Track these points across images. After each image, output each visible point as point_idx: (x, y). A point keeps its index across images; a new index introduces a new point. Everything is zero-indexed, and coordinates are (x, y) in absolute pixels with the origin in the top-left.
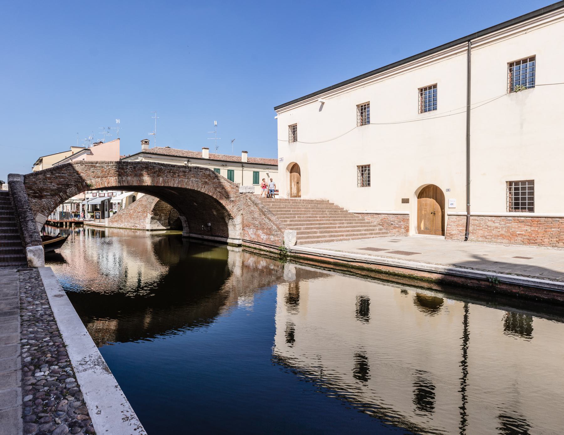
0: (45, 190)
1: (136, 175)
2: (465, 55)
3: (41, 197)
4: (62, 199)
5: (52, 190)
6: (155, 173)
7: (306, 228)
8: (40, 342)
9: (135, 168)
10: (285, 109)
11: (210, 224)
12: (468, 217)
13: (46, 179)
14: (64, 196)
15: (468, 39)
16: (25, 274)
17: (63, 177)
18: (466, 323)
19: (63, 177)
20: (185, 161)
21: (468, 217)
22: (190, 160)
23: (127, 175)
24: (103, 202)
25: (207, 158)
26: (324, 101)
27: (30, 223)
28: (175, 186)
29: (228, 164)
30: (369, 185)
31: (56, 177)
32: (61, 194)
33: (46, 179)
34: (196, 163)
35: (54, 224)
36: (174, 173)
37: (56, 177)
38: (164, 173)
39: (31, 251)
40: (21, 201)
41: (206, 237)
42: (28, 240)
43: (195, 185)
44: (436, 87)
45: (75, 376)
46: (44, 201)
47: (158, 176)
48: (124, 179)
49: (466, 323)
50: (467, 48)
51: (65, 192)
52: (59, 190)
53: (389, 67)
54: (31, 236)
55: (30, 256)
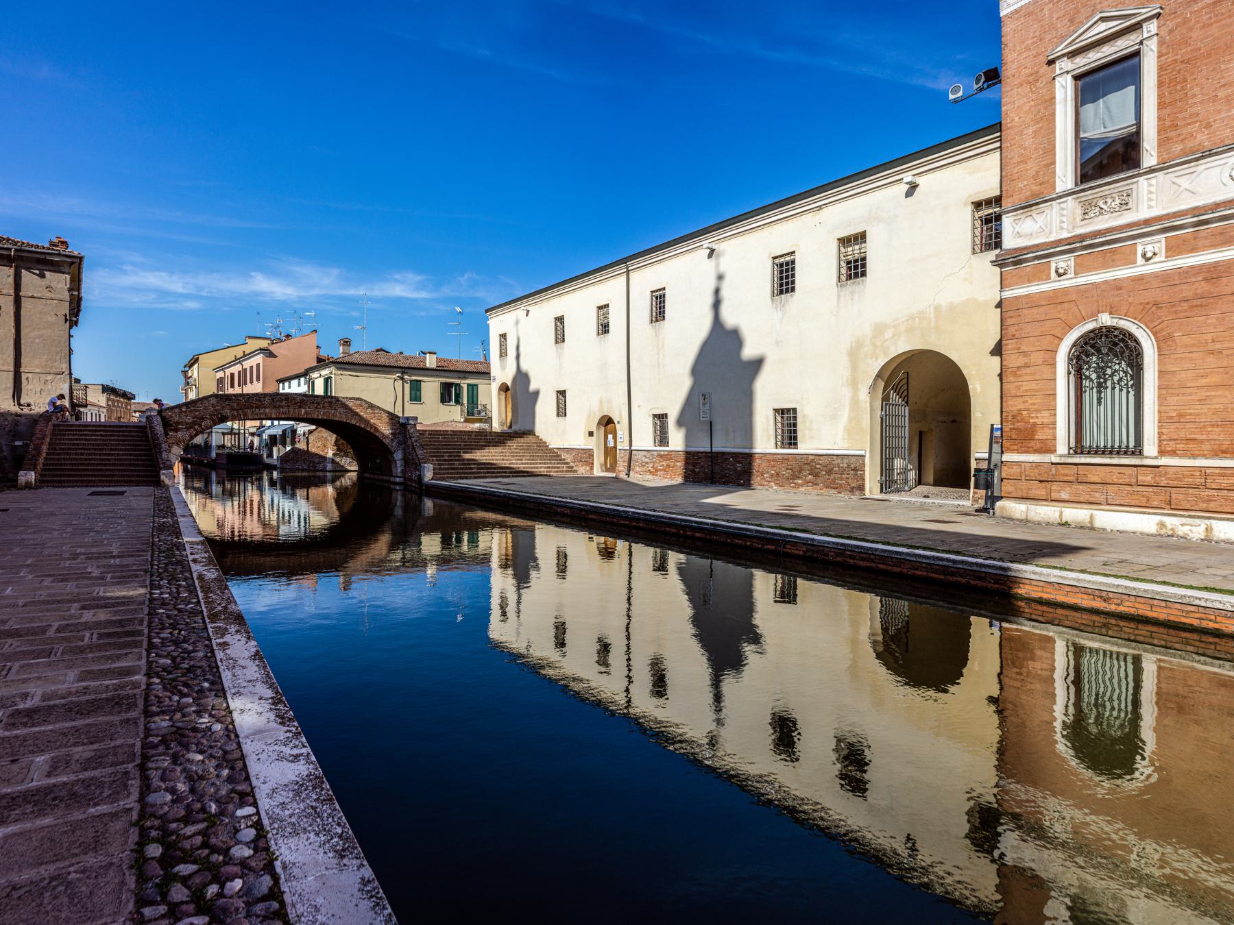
0: (182, 423)
1: (275, 407)
2: (623, 278)
3: (176, 430)
4: (197, 432)
5: (188, 424)
6: (295, 404)
7: (454, 464)
8: (181, 669)
9: (273, 399)
10: (888, 177)
11: (378, 461)
12: (631, 451)
13: (181, 412)
14: (200, 429)
15: (624, 261)
16: (158, 492)
17: (198, 411)
18: (631, 573)
19: (198, 411)
20: (398, 372)
21: (631, 451)
22: (406, 371)
23: (265, 407)
24: (284, 432)
25: (434, 366)
26: (714, 246)
27: (164, 453)
28: (320, 417)
29: (466, 375)
30: (565, 415)
31: (191, 411)
32: (196, 427)
33: (181, 412)
34: (415, 375)
35: (862, 789)
36: (319, 404)
37: (191, 411)
38: (306, 404)
39: (164, 474)
40: (157, 434)
41: (377, 477)
42: (162, 466)
43: (344, 416)
44: (865, 238)
45: (257, 803)
46: (180, 434)
47: (300, 407)
48: (262, 411)
49: (631, 573)
50: (998, 144)
51: (200, 425)
52: (194, 423)
53: (740, 218)
54: (164, 463)
55: (163, 477)
